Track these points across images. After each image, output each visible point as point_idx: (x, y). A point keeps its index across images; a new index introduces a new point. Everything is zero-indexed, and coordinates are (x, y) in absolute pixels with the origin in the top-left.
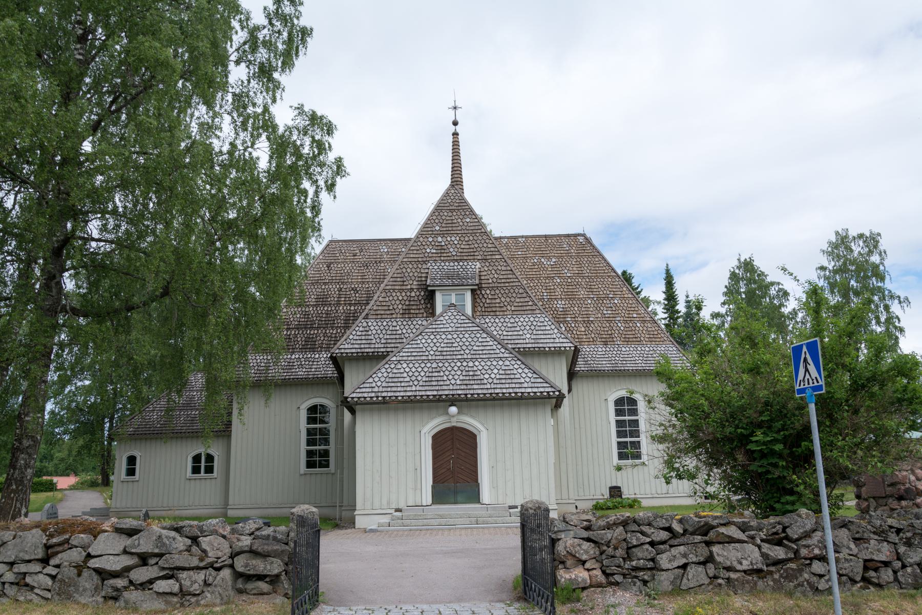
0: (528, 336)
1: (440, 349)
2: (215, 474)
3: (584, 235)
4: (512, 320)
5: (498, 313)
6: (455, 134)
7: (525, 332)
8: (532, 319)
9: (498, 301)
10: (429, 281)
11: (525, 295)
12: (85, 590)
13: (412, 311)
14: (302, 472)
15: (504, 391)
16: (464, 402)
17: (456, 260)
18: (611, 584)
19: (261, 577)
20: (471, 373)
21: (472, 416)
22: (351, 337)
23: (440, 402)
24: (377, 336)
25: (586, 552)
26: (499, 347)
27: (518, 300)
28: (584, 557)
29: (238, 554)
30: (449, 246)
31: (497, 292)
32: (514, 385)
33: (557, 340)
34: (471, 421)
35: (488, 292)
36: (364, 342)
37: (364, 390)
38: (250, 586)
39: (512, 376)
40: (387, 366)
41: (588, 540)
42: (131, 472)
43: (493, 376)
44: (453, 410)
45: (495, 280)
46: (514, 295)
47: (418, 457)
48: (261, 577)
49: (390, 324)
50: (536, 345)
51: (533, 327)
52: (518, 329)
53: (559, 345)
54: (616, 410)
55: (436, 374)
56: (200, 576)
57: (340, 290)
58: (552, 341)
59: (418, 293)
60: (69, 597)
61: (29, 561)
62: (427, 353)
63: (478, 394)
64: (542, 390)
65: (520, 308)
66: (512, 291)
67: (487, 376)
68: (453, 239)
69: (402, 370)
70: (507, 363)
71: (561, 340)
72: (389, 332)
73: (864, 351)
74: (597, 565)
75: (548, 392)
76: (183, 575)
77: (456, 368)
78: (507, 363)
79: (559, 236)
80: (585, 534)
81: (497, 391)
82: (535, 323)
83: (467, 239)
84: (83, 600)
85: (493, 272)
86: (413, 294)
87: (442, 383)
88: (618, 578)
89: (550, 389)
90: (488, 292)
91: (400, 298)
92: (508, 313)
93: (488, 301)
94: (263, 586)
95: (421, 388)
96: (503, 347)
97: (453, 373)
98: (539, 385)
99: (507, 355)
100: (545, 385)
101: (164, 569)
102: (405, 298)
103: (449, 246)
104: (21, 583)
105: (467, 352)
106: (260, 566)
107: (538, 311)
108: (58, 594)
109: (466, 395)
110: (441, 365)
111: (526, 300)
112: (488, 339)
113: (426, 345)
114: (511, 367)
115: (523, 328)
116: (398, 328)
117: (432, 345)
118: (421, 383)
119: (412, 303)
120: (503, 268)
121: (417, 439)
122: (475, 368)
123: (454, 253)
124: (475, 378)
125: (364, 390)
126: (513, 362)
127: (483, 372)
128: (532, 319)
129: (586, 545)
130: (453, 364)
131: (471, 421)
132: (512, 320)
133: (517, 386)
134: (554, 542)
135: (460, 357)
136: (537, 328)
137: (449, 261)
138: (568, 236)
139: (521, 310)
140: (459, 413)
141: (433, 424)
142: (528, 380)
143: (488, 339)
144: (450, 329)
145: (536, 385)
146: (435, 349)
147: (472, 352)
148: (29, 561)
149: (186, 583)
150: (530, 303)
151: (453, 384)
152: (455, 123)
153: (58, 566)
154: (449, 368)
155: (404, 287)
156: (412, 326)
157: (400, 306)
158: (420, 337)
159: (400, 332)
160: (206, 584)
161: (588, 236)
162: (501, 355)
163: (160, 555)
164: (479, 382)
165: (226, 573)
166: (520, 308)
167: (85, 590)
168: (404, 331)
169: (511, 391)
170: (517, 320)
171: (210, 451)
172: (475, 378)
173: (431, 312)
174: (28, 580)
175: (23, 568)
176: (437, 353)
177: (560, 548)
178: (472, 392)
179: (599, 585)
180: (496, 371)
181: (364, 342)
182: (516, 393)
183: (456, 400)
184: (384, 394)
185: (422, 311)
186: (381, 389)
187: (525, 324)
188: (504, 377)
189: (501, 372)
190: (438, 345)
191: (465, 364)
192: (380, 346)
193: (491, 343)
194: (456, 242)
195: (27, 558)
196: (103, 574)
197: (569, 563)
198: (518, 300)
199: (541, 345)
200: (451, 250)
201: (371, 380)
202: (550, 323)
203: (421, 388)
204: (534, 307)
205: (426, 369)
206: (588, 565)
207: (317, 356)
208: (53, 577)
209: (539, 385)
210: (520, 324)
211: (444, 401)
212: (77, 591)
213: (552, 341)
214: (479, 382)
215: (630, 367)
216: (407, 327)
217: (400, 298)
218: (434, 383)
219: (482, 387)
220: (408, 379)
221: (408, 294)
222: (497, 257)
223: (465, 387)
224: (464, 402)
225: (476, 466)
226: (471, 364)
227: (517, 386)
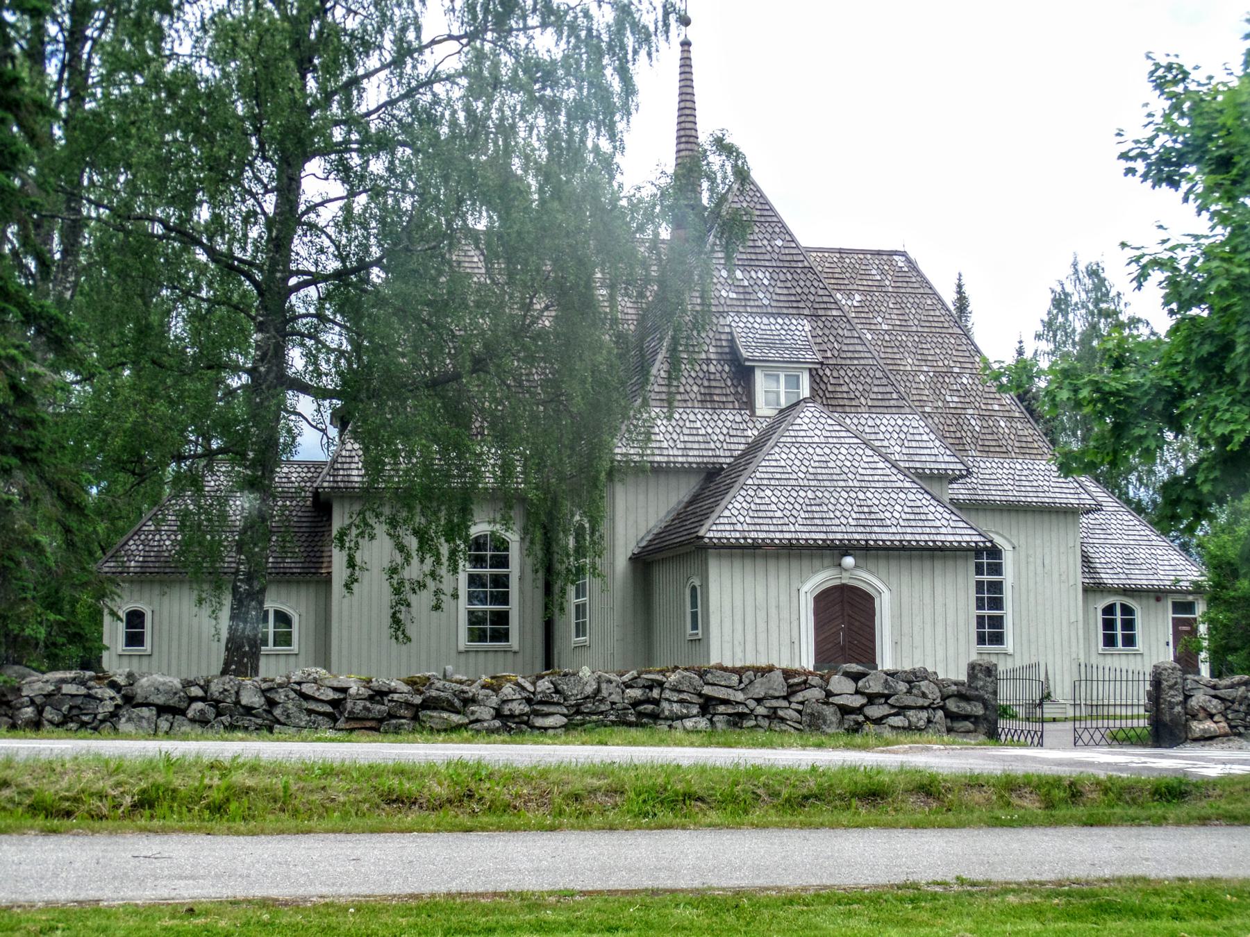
0: (898, 449)
2: (295, 647)
3: (903, 254)
4: (870, 422)
5: (848, 409)
8: (900, 422)
9: (845, 388)
11: (884, 381)
12: (832, 723)
13: (716, 398)
14: (462, 647)
15: (918, 537)
16: (868, 551)
17: (772, 314)
18: (1235, 735)
19: (966, 717)
21: (872, 573)
23: (834, 551)
24: (668, 437)
25: (1215, 707)
27: (875, 389)
28: (1214, 711)
29: (949, 697)
30: (756, 288)
31: (842, 373)
32: (928, 530)
33: (940, 459)
35: (828, 372)
37: (722, 527)
38: (957, 725)
39: (923, 517)
41: (1215, 697)
42: (134, 639)
45: (836, 354)
46: (869, 380)
47: (795, 624)
48: (966, 717)
49: (685, 416)
50: (911, 465)
51: (903, 436)
53: (943, 466)
55: (818, 508)
56: (924, 715)
58: (933, 458)
59: (719, 368)
60: (818, 728)
61: (777, 698)
65: (880, 403)
66: (864, 373)
67: (889, 515)
68: (760, 275)
70: (911, 496)
71: (947, 459)
72: (686, 431)
73: (428, 98)
74: (1222, 719)
76: (911, 713)
78: (911, 496)
79: (864, 252)
80: (1213, 692)
81: (908, 537)
83: (782, 277)
84: (829, 731)
85: (832, 339)
87: (828, 522)
88: (1242, 730)
89: (977, 538)
92: (863, 409)
93: (830, 388)
94: (969, 725)
95: (801, 528)
97: (839, 506)
98: (963, 532)
99: (907, 485)
100: (970, 532)
101: (893, 706)
103: (756, 288)
104: (773, 715)
106: (968, 708)
107: (908, 410)
108: (809, 726)
109: (866, 541)
116: (698, 425)
117: (797, 462)
119: (713, 384)
120: (847, 333)
121: (795, 600)
123: (766, 302)
124: (873, 516)
125: (722, 527)
126: (920, 496)
128: (900, 422)
129: (1215, 701)
132: (870, 422)
133: (933, 531)
134: (1187, 697)
137: (761, 315)
138: (879, 253)
139: (881, 406)
140: (856, 566)
141: (820, 579)
143: (876, 459)
145: (958, 531)
147: (859, 477)
148: (777, 698)
149: (914, 720)
151: (844, 528)
153: (802, 703)
156: (720, 423)
157: (695, 388)
159: (702, 431)
160: (929, 721)
161: (912, 256)
162: (899, 484)
163: (887, 697)
164: (879, 523)
165: (940, 713)
166: (880, 403)
167: (832, 723)
168: (710, 431)
169: (927, 538)
170: (878, 422)
171: (285, 608)
172: (873, 516)
174: (780, 713)
175: (775, 703)
176: (809, 476)
177: (1193, 702)
179: (1226, 735)
180: (898, 508)
182: (934, 542)
183: (855, 548)
184: (753, 535)
185: (731, 398)
186: (746, 527)
188: (912, 517)
189: (907, 510)
192: (676, 453)
194: (766, 282)
195: (777, 694)
196: (844, 710)
197: (1201, 715)
198: (875, 389)
199: (918, 465)
200: (761, 295)
203: (801, 528)
204: (902, 403)
206: (1216, 718)
208: (799, 712)
209: (963, 532)
212: (825, 722)
213: (933, 458)
214: (879, 523)
215: (996, 496)
216: (712, 424)
218: (818, 522)
219: (885, 530)
221: (705, 367)
222: (835, 313)
223: (862, 529)
224: (868, 551)
225: (873, 641)
226: (861, 496)
227: (933, 531)
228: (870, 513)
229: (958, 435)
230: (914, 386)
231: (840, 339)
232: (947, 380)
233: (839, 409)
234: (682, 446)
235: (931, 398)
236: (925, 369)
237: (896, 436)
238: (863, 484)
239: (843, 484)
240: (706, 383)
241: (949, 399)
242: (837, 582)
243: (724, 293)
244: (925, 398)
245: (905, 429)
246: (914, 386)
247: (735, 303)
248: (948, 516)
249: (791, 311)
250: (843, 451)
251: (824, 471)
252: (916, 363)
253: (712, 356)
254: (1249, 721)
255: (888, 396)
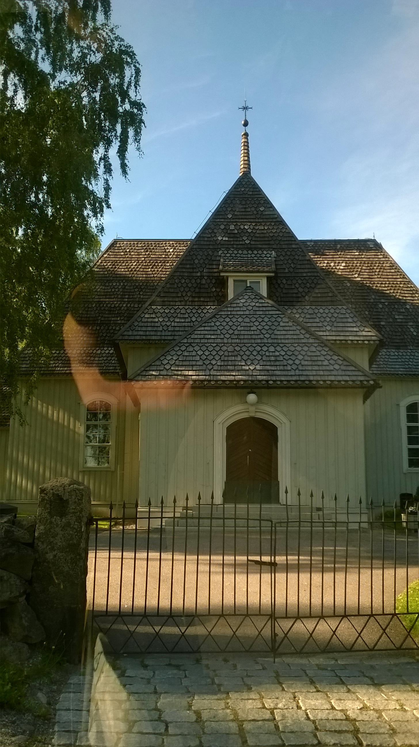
1: (236, 332)
4: (311, 311)
6: (246, 135)
7: (325, 324)
8: (332, 311)
10: (221, 267)
17: (250, 249)
20: (273, 358)
22: (136, 324)
26: (303, 332)
32: (321, 373)
34: (272, 412)
36: (150, 329)
39: (320, 363)
40: (177, 348)
43: (297, 362)
44: (252, 398)
45: (292, 270)
50: (338, 338)
52: (317, 320)
54: (408, 416)
57: (124, 287)
59: (209, 281)
62: (222, 336)
63: (281, 381)
64: (354, 378)
67: (290, 362)
69: (194, 353)
75: (361, 381)
77: (255, 353)
78: (314, 349)
82: (336, 315)
85: (290, 262)
86: (204, 282)
89: (362, 378)
90: (284, 281)
91: (190, 285)
96: (308, 332)
99: (311, 341)
102: (195, 285)
105: (267, 336)
110: (238, 349)
111: (326, 291)
112: (290, 324)
113: (221, 328)
114: (318, 353)
115: (323, 320)
117: (227, 327)
118: (216, 367)
119: (202, 290)
120: (300, 258)
122: (277, 354)
124: (277, 363)
126: (319, 348)
127: (286, 357)
130: (251, 349)
131: (272, 412)
135: (259, 341)
136: (338, 320)
141: (233, 411)
142: (337, 367)
144: (247, 312)
146: (231, 332)
147: (273, 336)
150: (330, 295)
152: (246, 124)
154: (248, 353)
155: (194, 274)
158: (214, 320)
164: (282, 368)
169: (319, 378)
170: (316, 311)
173: (221, 298)
178: (274, 378)
181: (150, 329)
182: (324, 381)
187: (324, 315)
190: (234, 328)
191: (265, 348)
193: (294, 328)
200: (245, 238)
201: (158, 363)
202: (352, 315)
205: (221, 353)
207: (99, 352)
210: (319, 315)
211: (242, 387)
217: (190, 285)
220: (200, 363)
226: (272, 349)
227: (326, 373)
228: (276, 361)
229: (402, 337)
230: (375, 310)
231: (295, 262)
232: (396, 306)
233: (288, 304)
234: (172, 329)
235: (386, 317)
236: (383, 301)
237: (328, 319)
238: (275, 341)
239: (259, 341)
240: (197, 290)
241: (397, 317)
242: (245, 415)
243: (220, 238)
244: (381, 317)
245: (336, 315)
246: (375, 310)
247: (226, 243)
248: (340, 362)
249: (264, 246)
250: (266, 319)
251: (246, 333)
252: (377, 298)
253: (205, 274)
254: (407, 522)
255: (326, 295)
